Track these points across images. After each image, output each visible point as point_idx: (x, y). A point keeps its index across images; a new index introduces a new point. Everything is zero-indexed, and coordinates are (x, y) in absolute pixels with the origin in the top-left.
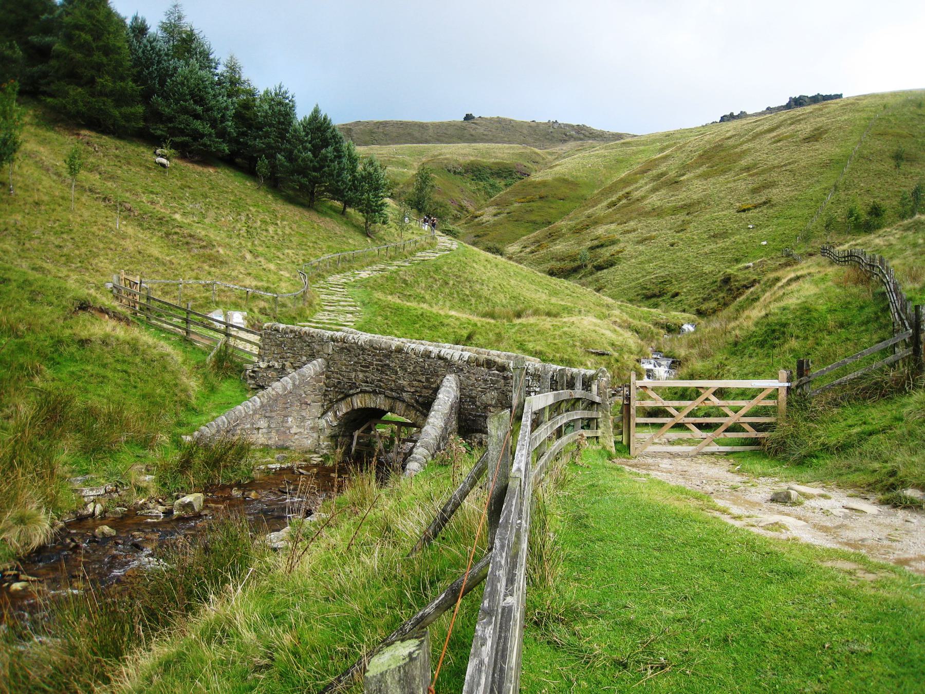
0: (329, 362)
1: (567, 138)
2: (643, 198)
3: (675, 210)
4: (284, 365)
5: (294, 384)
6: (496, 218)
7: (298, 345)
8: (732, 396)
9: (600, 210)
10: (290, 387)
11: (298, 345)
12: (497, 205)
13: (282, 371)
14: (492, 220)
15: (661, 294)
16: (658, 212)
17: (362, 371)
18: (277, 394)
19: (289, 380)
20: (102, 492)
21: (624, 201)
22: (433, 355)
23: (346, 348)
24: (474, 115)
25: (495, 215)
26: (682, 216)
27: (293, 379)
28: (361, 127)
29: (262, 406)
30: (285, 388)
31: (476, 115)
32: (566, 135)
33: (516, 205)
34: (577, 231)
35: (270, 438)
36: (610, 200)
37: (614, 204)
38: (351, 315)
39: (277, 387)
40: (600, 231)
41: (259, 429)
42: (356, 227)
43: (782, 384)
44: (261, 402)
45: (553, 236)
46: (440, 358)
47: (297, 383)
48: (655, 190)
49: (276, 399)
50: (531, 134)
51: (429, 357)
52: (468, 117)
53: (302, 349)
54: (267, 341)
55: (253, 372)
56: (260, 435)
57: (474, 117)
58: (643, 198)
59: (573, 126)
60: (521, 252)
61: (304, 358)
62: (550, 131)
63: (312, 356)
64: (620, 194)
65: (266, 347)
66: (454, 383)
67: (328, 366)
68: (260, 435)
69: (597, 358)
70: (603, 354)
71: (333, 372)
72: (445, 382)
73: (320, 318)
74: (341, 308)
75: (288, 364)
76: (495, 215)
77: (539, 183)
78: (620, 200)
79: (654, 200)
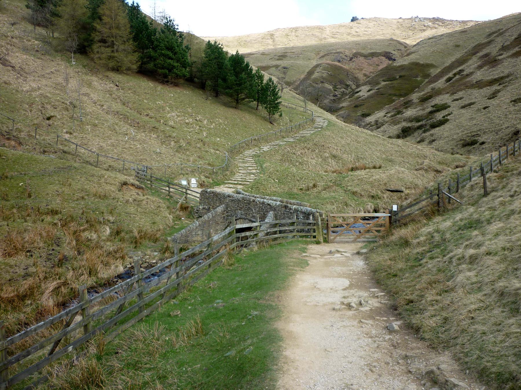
0: (227, 206)
1: (425, 28)
2: (471, 74)
3: (491, 83)
4: (209, 207)
5: (213, 216)
6: (369, 93)
7: (215, 198)
8: (517, 213)
9: (440, 83)
10: (211, 217)
11: (215, 198)
12: (370, 84)
13: (209, 210)
14: (366, 95)
15: (473, 143)
16: (480, 85)
17: (240, 210)
18: (206, 220)
19: (210, 214)
20: (139, 258)
21: (458, 77)
22: (266, 203)
23: (233, 200)
24: (358, 17)
25: (369, 91)
26: (495, 87)
27: (212, 214)
28: (280, 32)
29: (199, 225)
30: (209, 218)
31: (359, 17)
32: (425, 26)
33: (383, 83)
34: (424, 100)
35: (203, 238)
36: (448, 76)
37: (449, 80)
38: (253, 175)
39: (206, 217)
40: (438, 100)
41: (198, 235)
42: (265, 119)
43: (386, 215)
44: (199, 224)
45: (407, 105)
46: (269, 205)
47: (214, 215)
48: (480, 67)
49: (205, 223)
50: (398, 28)
51: (264, 203)
52: (354, 19)
53: (217, 200)
54: (203, 196)
55: (197, 210)
56: (199, 237)
57: (358, 19)
58: (471, 74)
59: (430, 19)
60: (385, 116)
61: (218, 204)
62: (413, 24)
63: (221, 203)
64: (455, 71)
65: (203, 199)
66: (273, 215)
67: (227, 208)
68: (199, 237)
69: (391, 193)
70: (400, 191)
71: (229, 210)
72: (269, 215)
73: (237, 177)
74: (249, 171)
75: (211, 207)
76: (369, 91)
77: (399, 67)
78: (455, 75)
79: (479, 76)
